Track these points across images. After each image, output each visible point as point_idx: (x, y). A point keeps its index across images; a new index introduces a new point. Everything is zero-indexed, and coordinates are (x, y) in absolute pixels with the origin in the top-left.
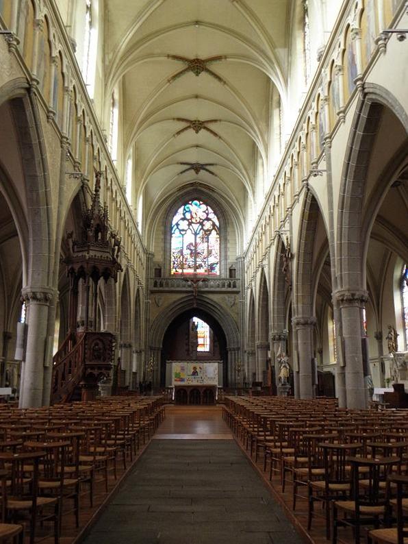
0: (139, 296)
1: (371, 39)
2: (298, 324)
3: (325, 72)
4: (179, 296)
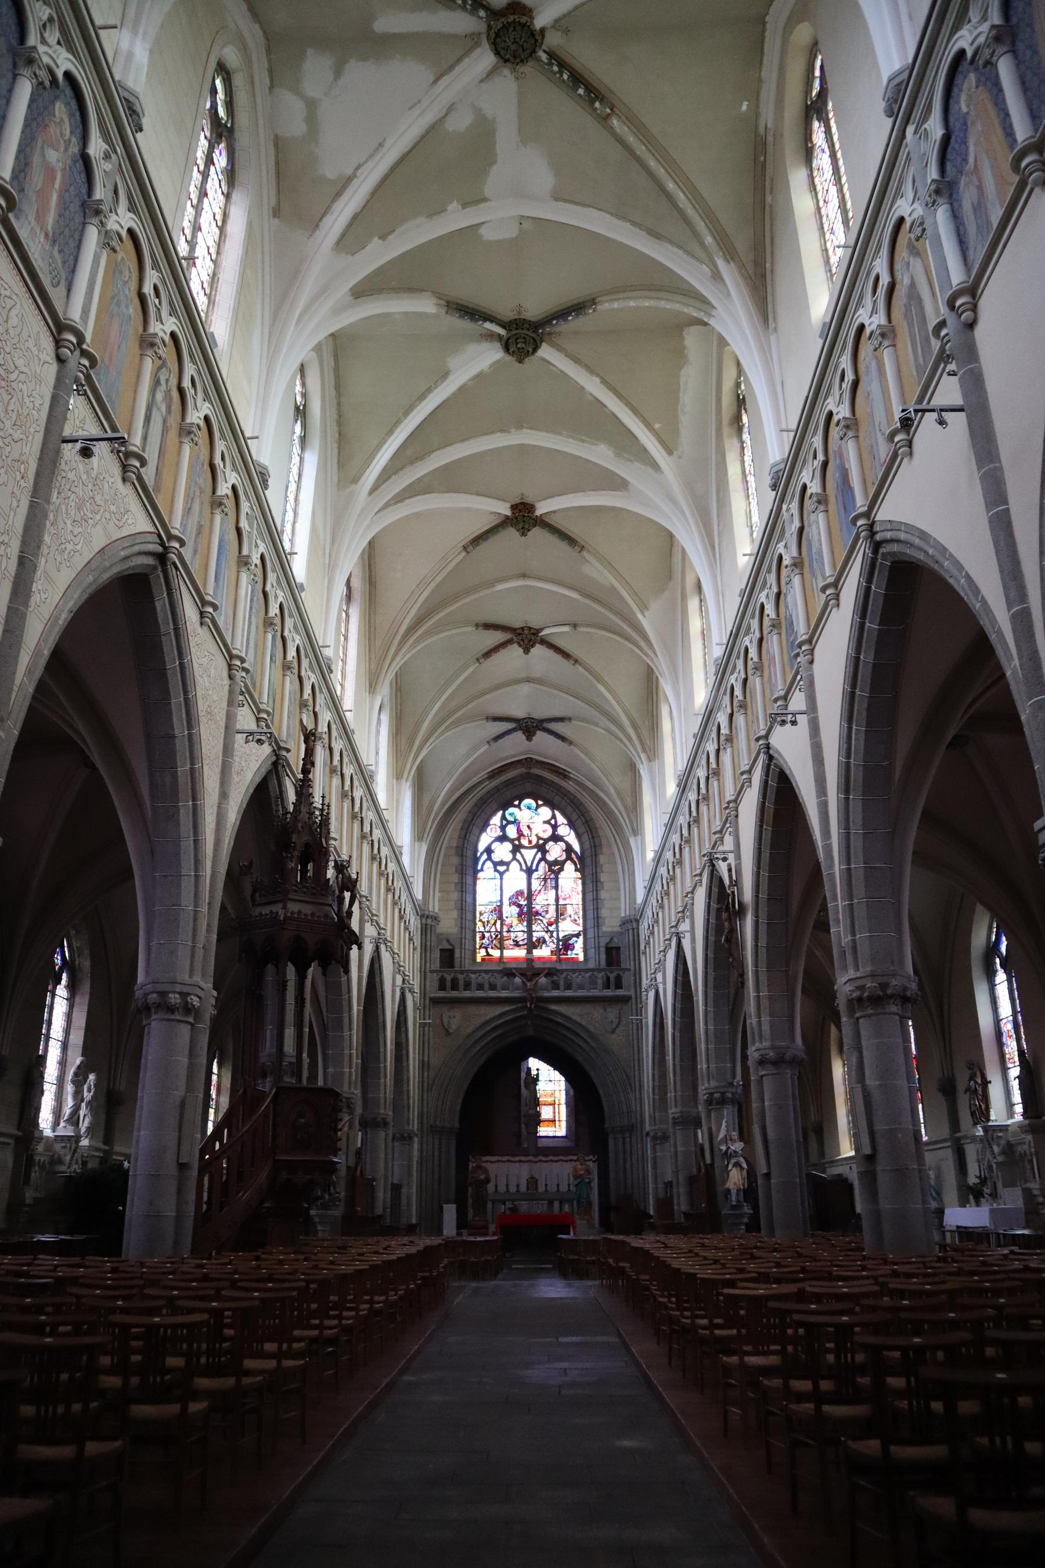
0: (405, 1008)
1: (879, 435)
2: (762, 1062)
3: (788, 510)
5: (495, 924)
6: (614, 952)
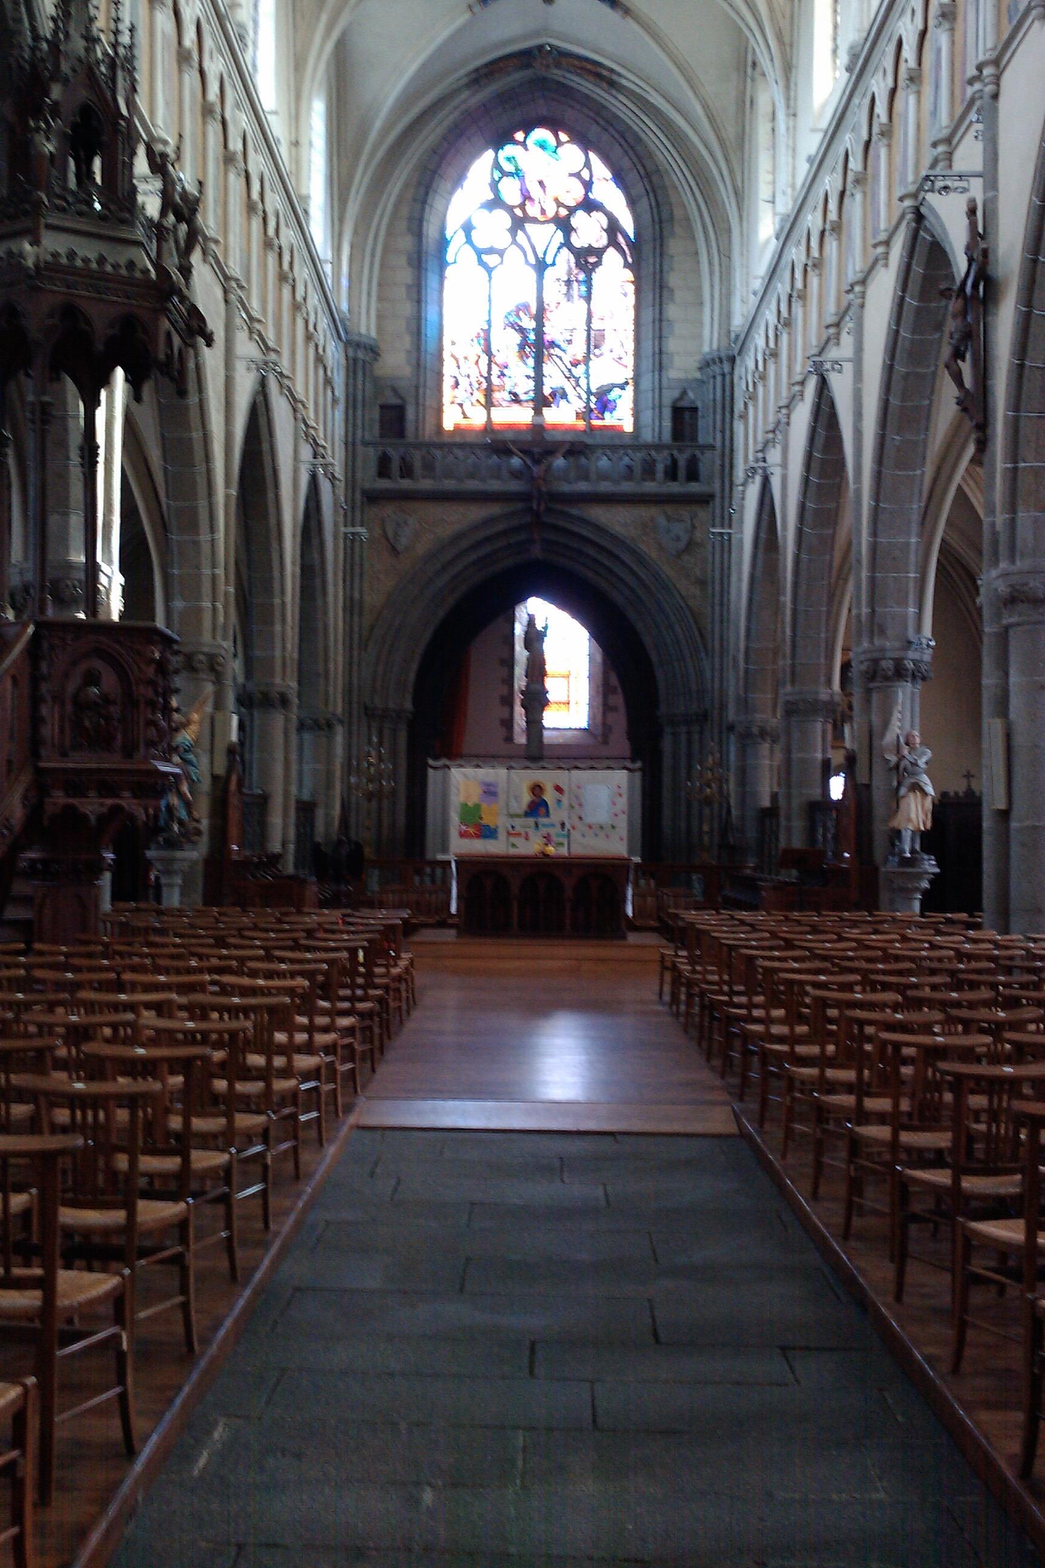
4: (476, 513)
6: (687, 415)
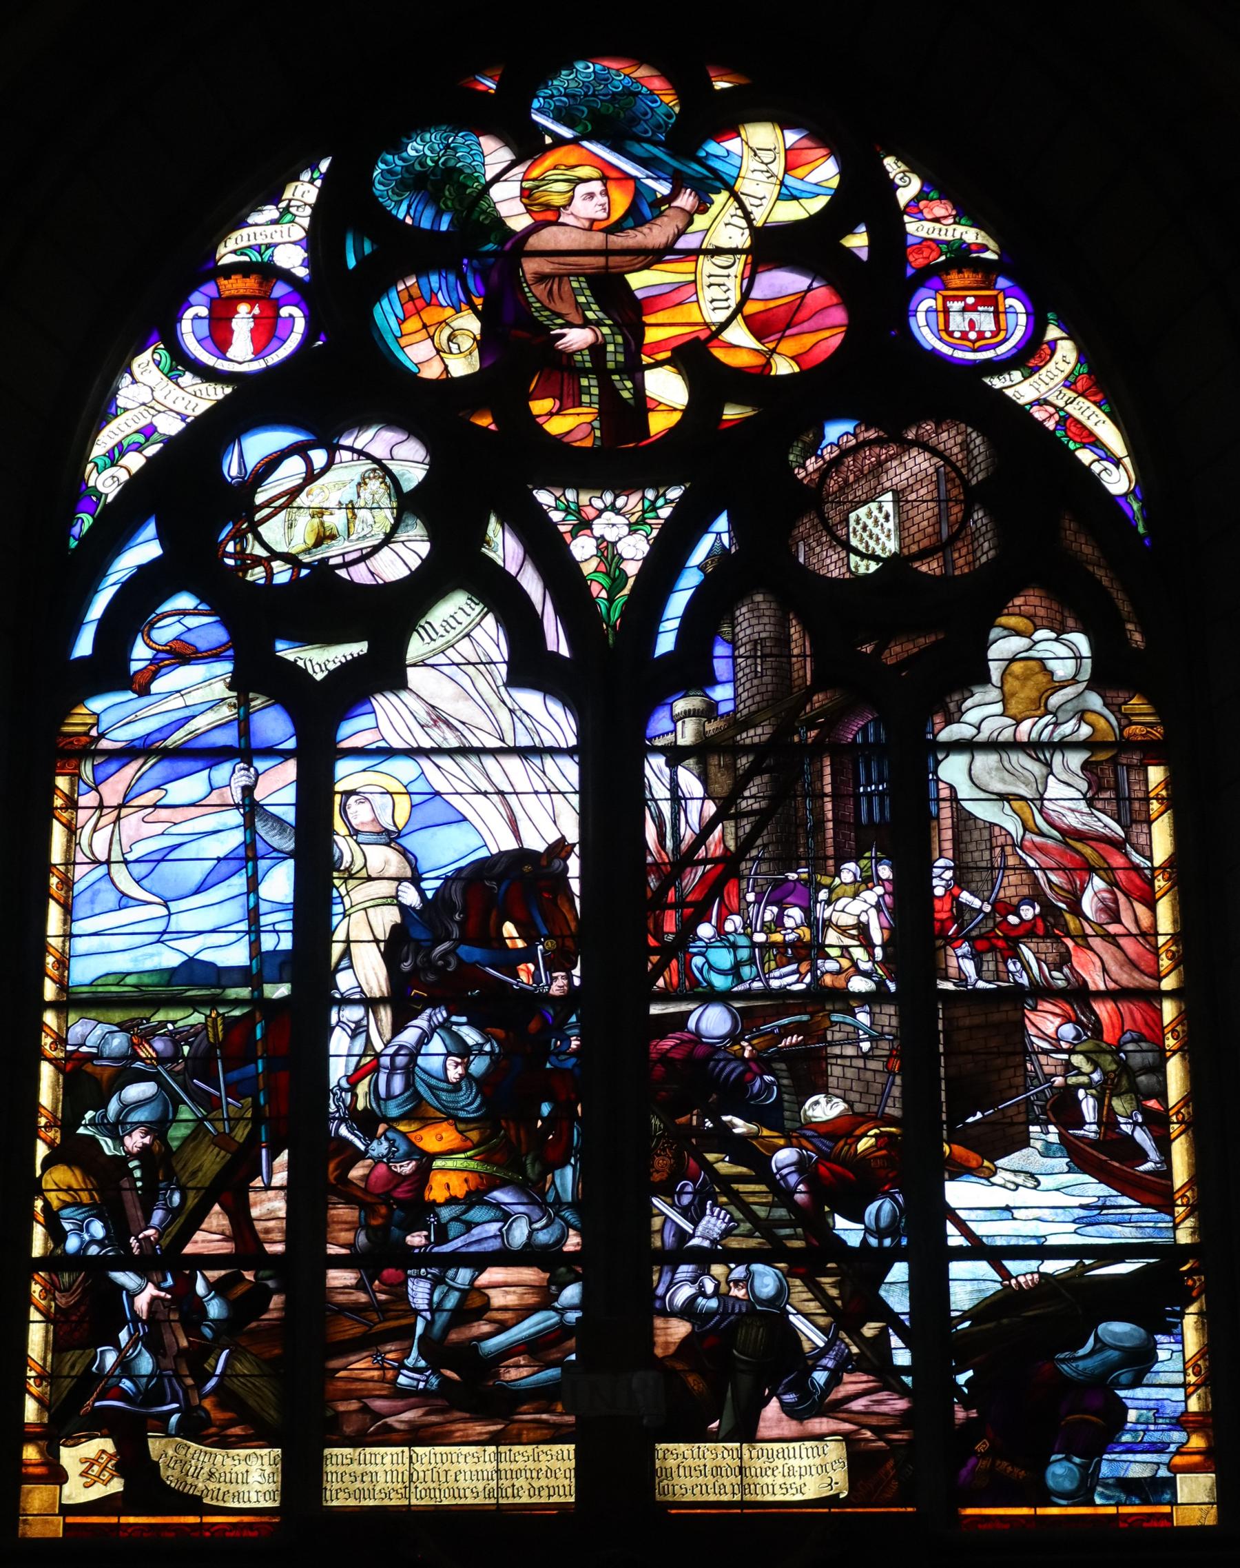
5: (232, 1190)
